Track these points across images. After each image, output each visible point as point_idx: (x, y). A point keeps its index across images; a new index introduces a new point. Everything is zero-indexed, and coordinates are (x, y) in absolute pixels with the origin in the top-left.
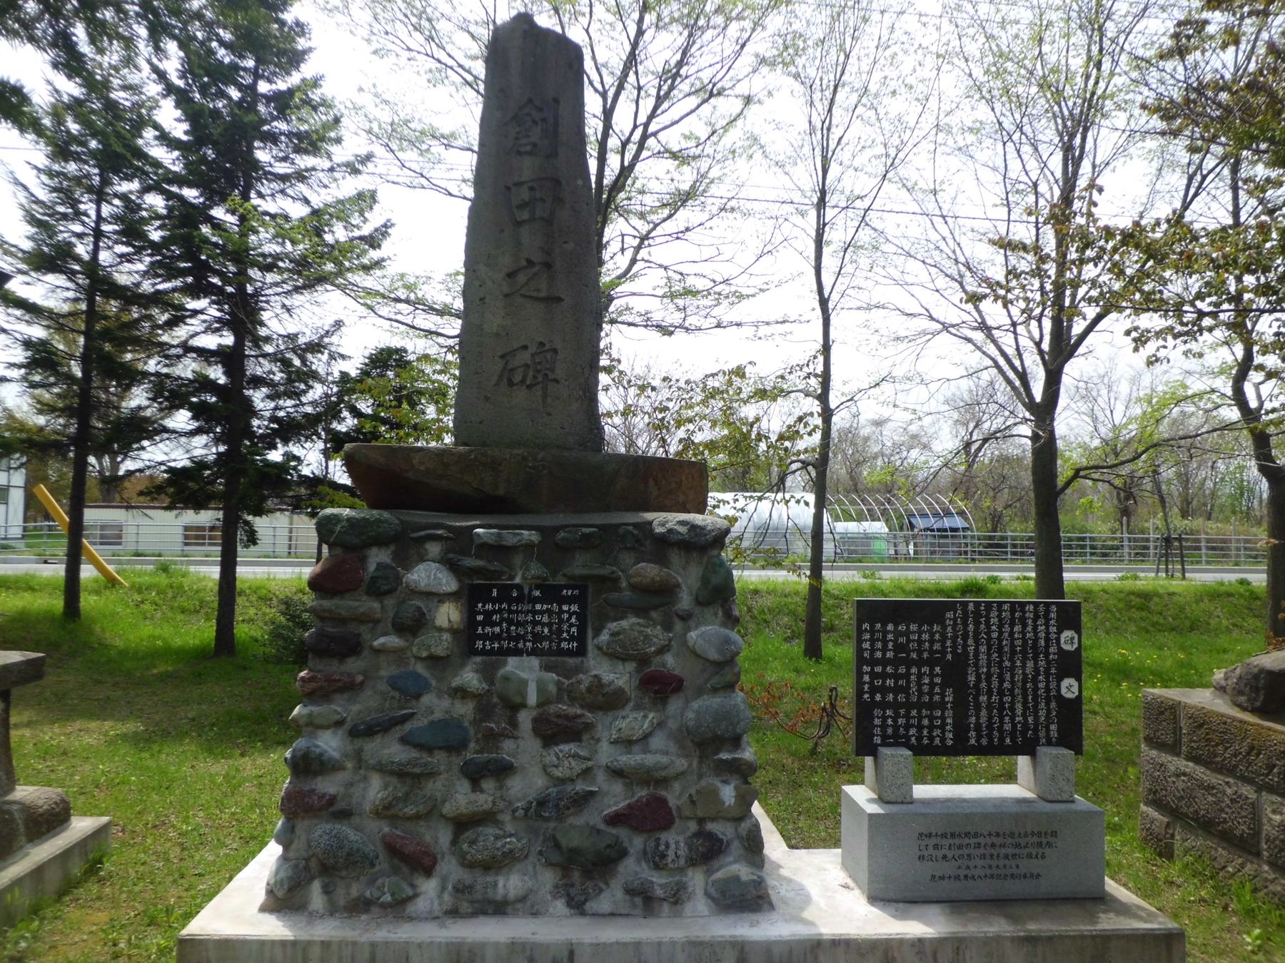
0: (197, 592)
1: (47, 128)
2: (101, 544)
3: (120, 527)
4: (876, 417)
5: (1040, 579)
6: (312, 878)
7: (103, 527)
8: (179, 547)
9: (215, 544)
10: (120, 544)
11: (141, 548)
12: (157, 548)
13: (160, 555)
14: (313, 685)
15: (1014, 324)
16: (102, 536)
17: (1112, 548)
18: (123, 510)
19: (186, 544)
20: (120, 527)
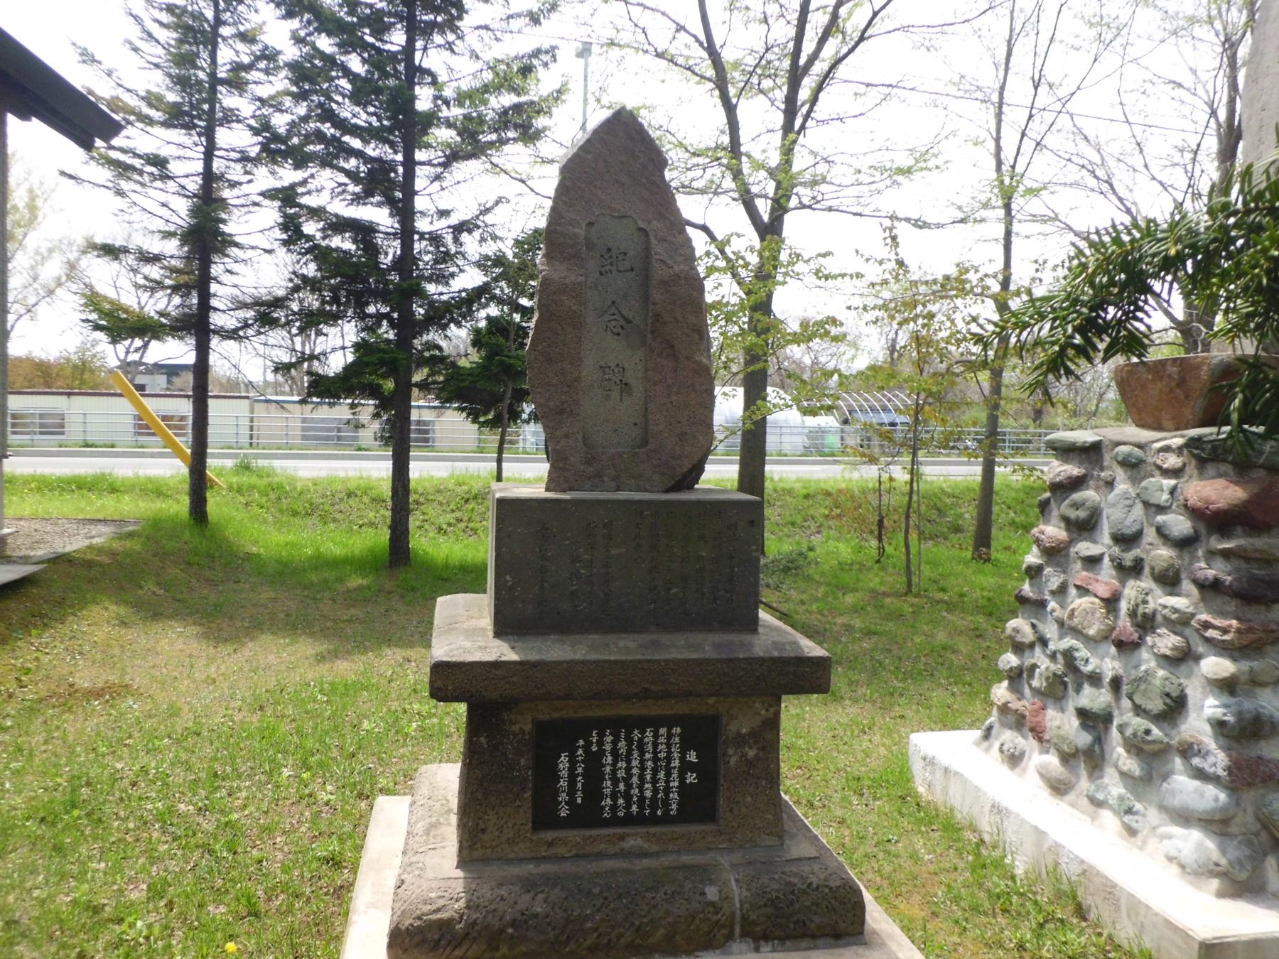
0: (301, 493)
1: (206, 20)
2: (41, 433)
3: (62, 417)
4: (109, 241)
5: (742, 474)
6: (1265, 855)
7: (42, 416)
8: (130, 438)
9: (730, 462)
10: (63, 433)
11: (89, 438)
12: (109, 438)
13: (113, 446)
14: (1251, 637)
15: (1069, 160)
16: (42, 425)
17: (1024, 442)
18: (65, 397)
19: (140, 434)
20: (62, 417)
